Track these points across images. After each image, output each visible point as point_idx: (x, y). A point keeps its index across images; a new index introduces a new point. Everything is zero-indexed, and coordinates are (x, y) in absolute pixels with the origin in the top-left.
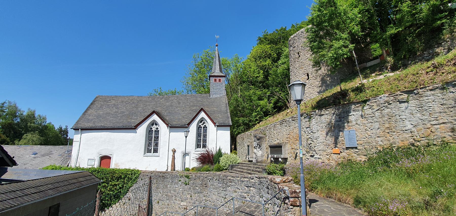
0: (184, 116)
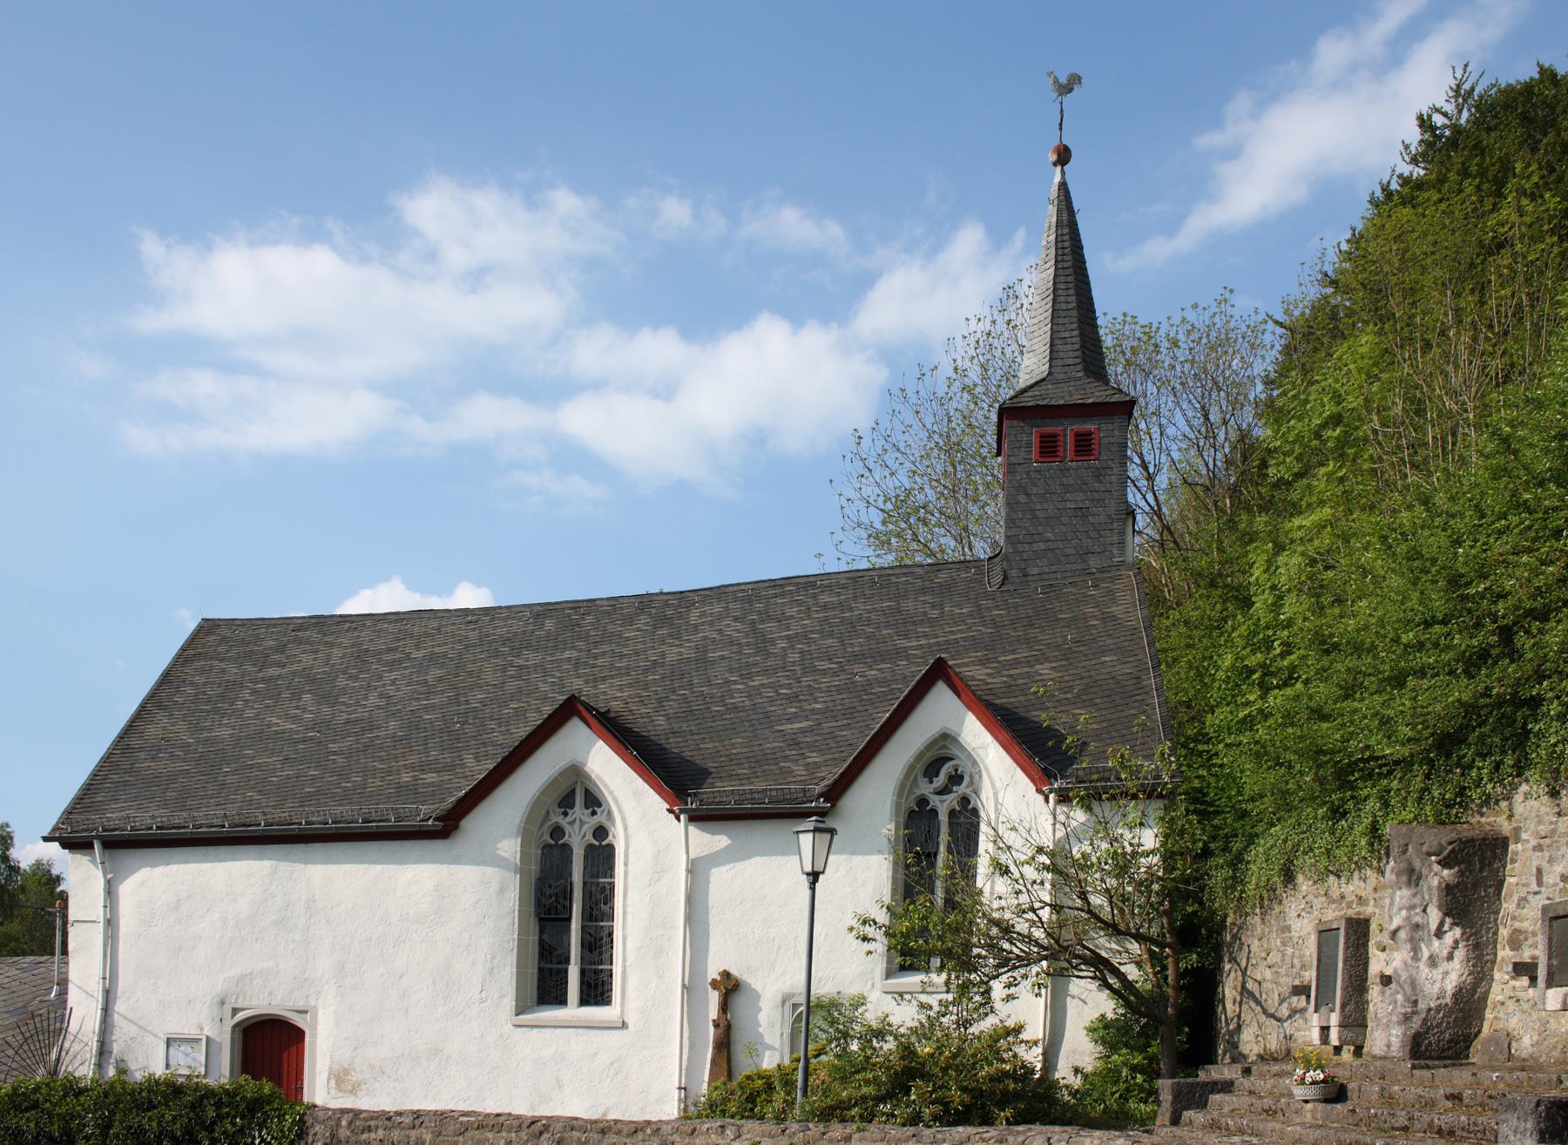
0: (803, 731)
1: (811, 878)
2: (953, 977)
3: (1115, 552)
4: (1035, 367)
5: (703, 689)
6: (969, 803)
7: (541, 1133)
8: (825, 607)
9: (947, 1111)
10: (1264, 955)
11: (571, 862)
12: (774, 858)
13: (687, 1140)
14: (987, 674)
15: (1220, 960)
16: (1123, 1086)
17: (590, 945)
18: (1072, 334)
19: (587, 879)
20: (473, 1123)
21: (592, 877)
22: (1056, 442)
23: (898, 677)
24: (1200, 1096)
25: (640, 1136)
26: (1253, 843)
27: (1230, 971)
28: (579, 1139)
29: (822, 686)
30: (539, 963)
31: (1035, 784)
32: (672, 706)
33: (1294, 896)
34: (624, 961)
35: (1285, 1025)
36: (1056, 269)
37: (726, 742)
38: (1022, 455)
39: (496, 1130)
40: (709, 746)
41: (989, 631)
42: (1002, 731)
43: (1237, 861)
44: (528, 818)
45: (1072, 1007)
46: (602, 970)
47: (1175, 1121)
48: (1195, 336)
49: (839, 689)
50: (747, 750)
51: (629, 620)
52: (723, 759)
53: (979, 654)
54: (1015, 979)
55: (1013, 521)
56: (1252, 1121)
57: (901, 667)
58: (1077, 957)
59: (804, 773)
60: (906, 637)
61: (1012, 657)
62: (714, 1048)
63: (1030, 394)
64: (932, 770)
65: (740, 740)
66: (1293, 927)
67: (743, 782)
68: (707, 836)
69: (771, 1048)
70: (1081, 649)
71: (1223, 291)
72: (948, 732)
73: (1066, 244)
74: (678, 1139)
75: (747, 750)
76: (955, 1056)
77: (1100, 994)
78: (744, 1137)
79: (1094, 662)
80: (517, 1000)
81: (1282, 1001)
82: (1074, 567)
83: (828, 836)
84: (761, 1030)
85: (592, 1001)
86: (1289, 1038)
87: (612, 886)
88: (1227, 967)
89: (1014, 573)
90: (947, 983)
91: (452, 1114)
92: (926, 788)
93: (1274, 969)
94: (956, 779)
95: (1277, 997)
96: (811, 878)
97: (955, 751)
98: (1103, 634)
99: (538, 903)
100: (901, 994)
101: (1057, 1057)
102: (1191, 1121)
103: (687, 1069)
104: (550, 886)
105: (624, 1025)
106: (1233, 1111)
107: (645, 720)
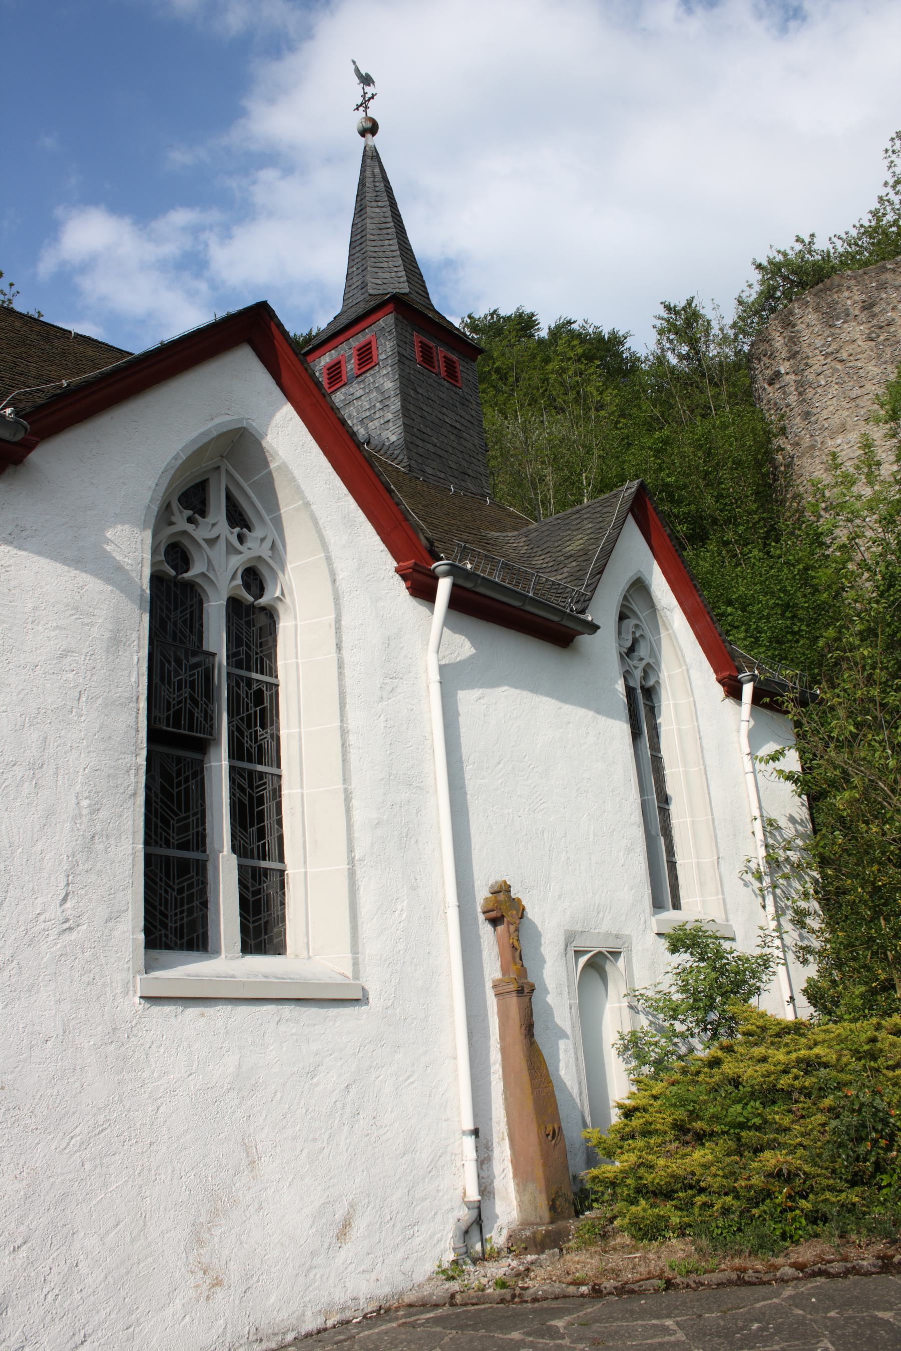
46: (266, 870)
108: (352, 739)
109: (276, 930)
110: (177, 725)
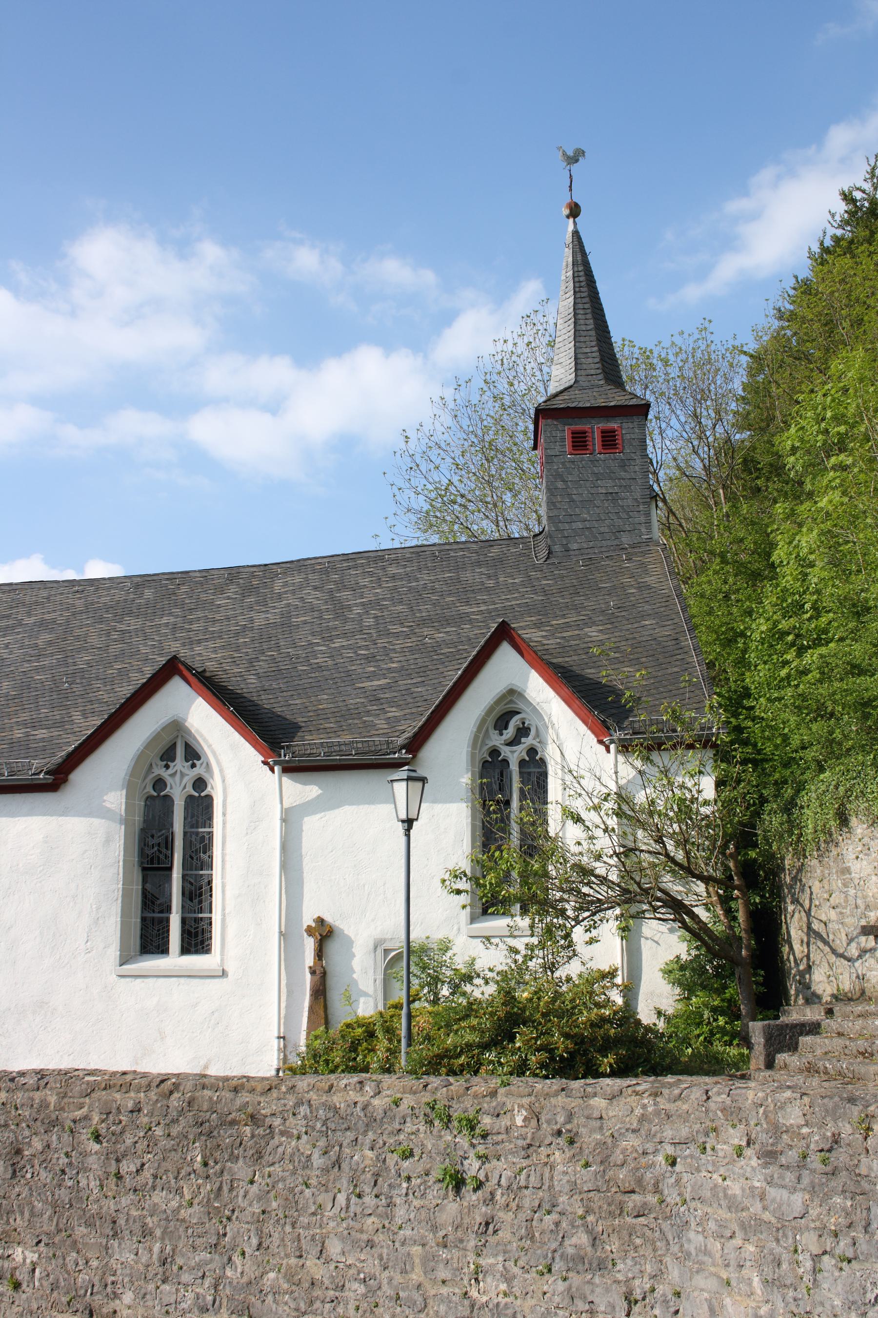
0: (382, 688)
1: (406, 825)
2: (537, 920)
3: (643, 530)
4: (562, 376)
5: (289, 650)
6: (537, 753)
7: (171, 1093)
8: (393, 577)
9: (552, 1059)
10: (826, 896)
11: (173, 812)
12: (361, 807)
13: (324, 1098)
14: (543, 637)
15: (782, 899)
16: (706, 1029)
17: (191, 893)
18: (592, 350)
19: (188, 830)
20: (99, 1083)
21: (192, 827)
22: (585, 437)
23: (464, 639)
24: (791, 1038)
25: (275, 1093)
26: (804, 789)
27: (794, 912)
28: (211, 1098)
29: (396, 647)
30: (142, 912)
31: (596, 735)
32: (262, 666)
33: (850, 839)
34: (224, 909)
35: (857, 964)
36: (575, 298)
37: (313, 699)
38: (557, 449)
39: (124, 1090)
40: (297, 702)
41: (540, 598)
42: (563, 686)
43: (789, 807)
44: (133, 771)
45: (646, 947)
46: (201, 919)
47: (770, 1064)
48: (684, 356)
49: (412, 650)
50: (332, 705)
51: (220, 590)
52: (311, 714)
53: (533, 618)
54: (595, 922)
55: (553, 504)
56: (852, 1064)
57: (465, 630)
58: (658, 899)
59: (386, 726)
60: (467, 603)
61: (563, 621)
62: (311, 995)
63: (560, 398)
64: (502, 721)
65: (325, 697)
66: (852, 869)
67: (330, 735)
68: (299, 786)
69: (366, 994)
70: (623, 614)
71: (703, 321)
72: (514, 688)
73: (582, 279)
74: (315, 1097)
75: (332, 705)
76: (554, 1000)
77: (672, 935)
78: (384, 1093)
79: (636, 625)
80: (121, 950)
81: (850, 941)
82: (609, 543)
83: (420, 784)
84: (355, 976)
85: (193, 949)
86: (861, 978)
87: (211, 834)
88: (791, 908)
89: (557, 548)
90: (532, 927)
91: (76, 1073)
92: (497, 740)
93: (838, 910)
94: (523, 731)
95: (844, 938)
96: (406, 825)
97: (521, 706)
98: (641, 601)
99: (142, 853)
100: (488, 938)
101: (636, 999)
102: (786, 1065)
103: (285, 1017)
104: (153, 836)
105: (224, 974)
106: (826, 1053)
107: (239, 679)
108: (227, 858)
109: (206, 943)
110: (152, 863)
